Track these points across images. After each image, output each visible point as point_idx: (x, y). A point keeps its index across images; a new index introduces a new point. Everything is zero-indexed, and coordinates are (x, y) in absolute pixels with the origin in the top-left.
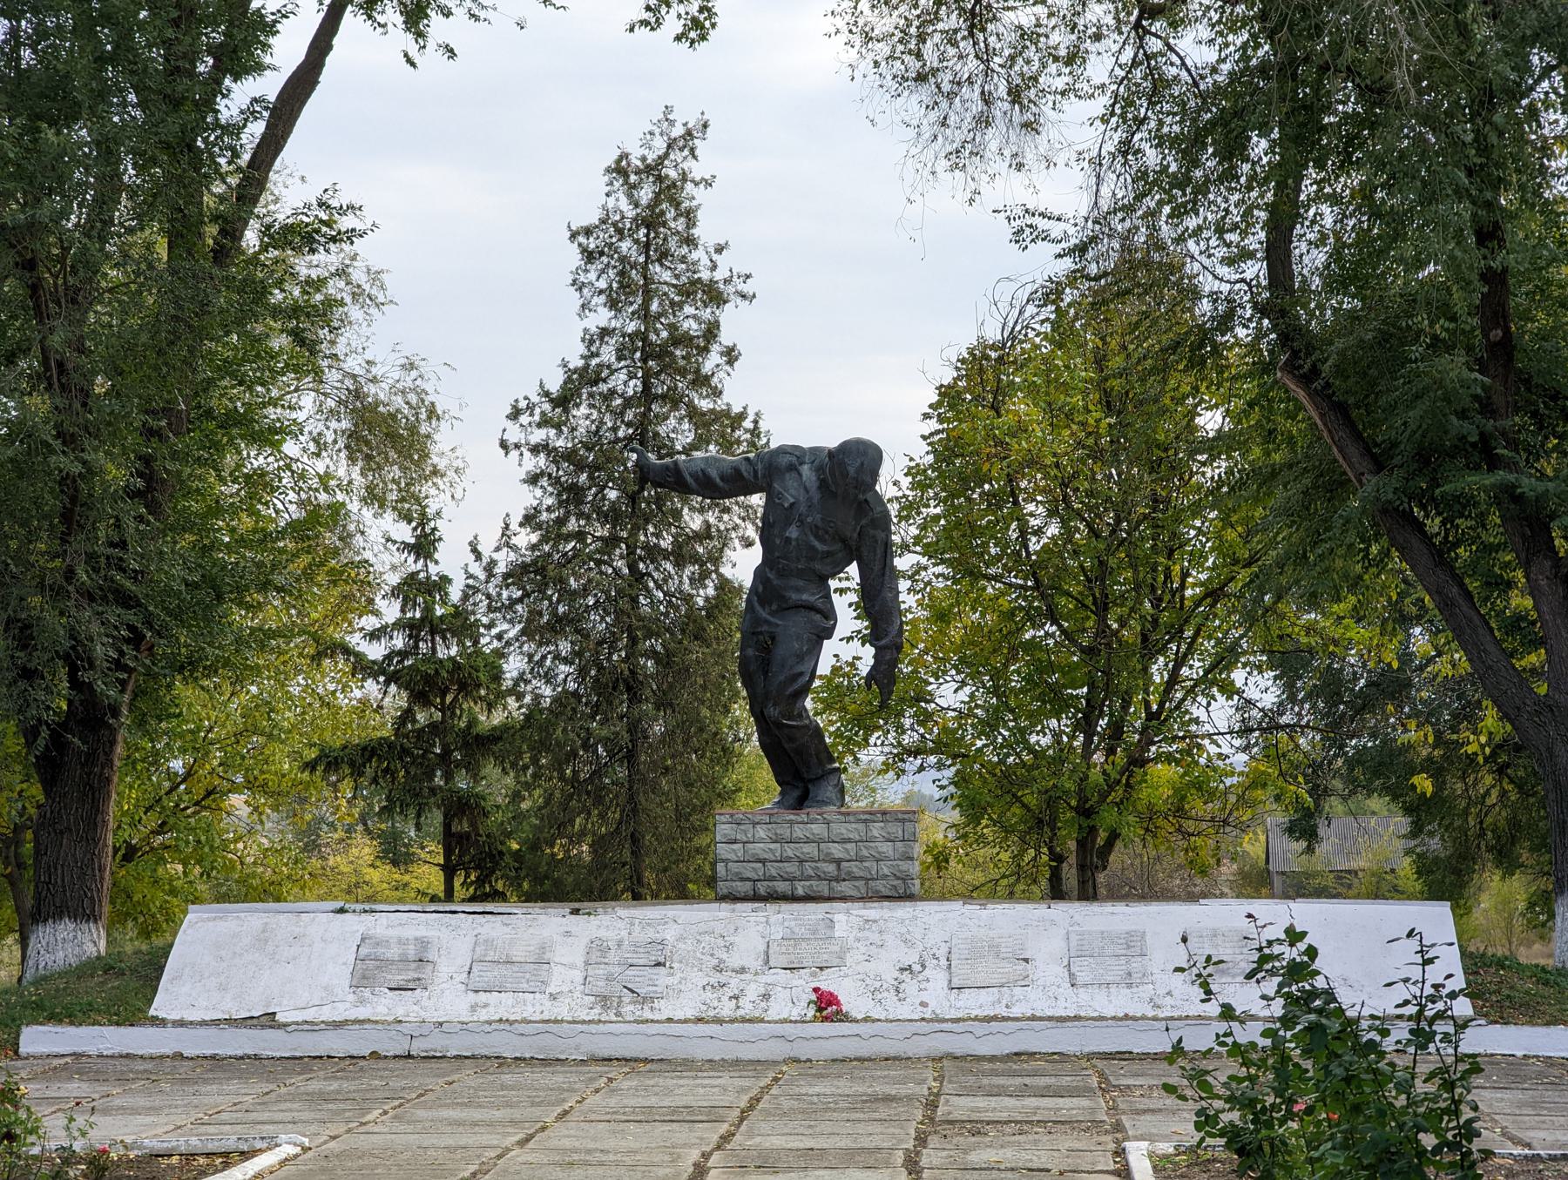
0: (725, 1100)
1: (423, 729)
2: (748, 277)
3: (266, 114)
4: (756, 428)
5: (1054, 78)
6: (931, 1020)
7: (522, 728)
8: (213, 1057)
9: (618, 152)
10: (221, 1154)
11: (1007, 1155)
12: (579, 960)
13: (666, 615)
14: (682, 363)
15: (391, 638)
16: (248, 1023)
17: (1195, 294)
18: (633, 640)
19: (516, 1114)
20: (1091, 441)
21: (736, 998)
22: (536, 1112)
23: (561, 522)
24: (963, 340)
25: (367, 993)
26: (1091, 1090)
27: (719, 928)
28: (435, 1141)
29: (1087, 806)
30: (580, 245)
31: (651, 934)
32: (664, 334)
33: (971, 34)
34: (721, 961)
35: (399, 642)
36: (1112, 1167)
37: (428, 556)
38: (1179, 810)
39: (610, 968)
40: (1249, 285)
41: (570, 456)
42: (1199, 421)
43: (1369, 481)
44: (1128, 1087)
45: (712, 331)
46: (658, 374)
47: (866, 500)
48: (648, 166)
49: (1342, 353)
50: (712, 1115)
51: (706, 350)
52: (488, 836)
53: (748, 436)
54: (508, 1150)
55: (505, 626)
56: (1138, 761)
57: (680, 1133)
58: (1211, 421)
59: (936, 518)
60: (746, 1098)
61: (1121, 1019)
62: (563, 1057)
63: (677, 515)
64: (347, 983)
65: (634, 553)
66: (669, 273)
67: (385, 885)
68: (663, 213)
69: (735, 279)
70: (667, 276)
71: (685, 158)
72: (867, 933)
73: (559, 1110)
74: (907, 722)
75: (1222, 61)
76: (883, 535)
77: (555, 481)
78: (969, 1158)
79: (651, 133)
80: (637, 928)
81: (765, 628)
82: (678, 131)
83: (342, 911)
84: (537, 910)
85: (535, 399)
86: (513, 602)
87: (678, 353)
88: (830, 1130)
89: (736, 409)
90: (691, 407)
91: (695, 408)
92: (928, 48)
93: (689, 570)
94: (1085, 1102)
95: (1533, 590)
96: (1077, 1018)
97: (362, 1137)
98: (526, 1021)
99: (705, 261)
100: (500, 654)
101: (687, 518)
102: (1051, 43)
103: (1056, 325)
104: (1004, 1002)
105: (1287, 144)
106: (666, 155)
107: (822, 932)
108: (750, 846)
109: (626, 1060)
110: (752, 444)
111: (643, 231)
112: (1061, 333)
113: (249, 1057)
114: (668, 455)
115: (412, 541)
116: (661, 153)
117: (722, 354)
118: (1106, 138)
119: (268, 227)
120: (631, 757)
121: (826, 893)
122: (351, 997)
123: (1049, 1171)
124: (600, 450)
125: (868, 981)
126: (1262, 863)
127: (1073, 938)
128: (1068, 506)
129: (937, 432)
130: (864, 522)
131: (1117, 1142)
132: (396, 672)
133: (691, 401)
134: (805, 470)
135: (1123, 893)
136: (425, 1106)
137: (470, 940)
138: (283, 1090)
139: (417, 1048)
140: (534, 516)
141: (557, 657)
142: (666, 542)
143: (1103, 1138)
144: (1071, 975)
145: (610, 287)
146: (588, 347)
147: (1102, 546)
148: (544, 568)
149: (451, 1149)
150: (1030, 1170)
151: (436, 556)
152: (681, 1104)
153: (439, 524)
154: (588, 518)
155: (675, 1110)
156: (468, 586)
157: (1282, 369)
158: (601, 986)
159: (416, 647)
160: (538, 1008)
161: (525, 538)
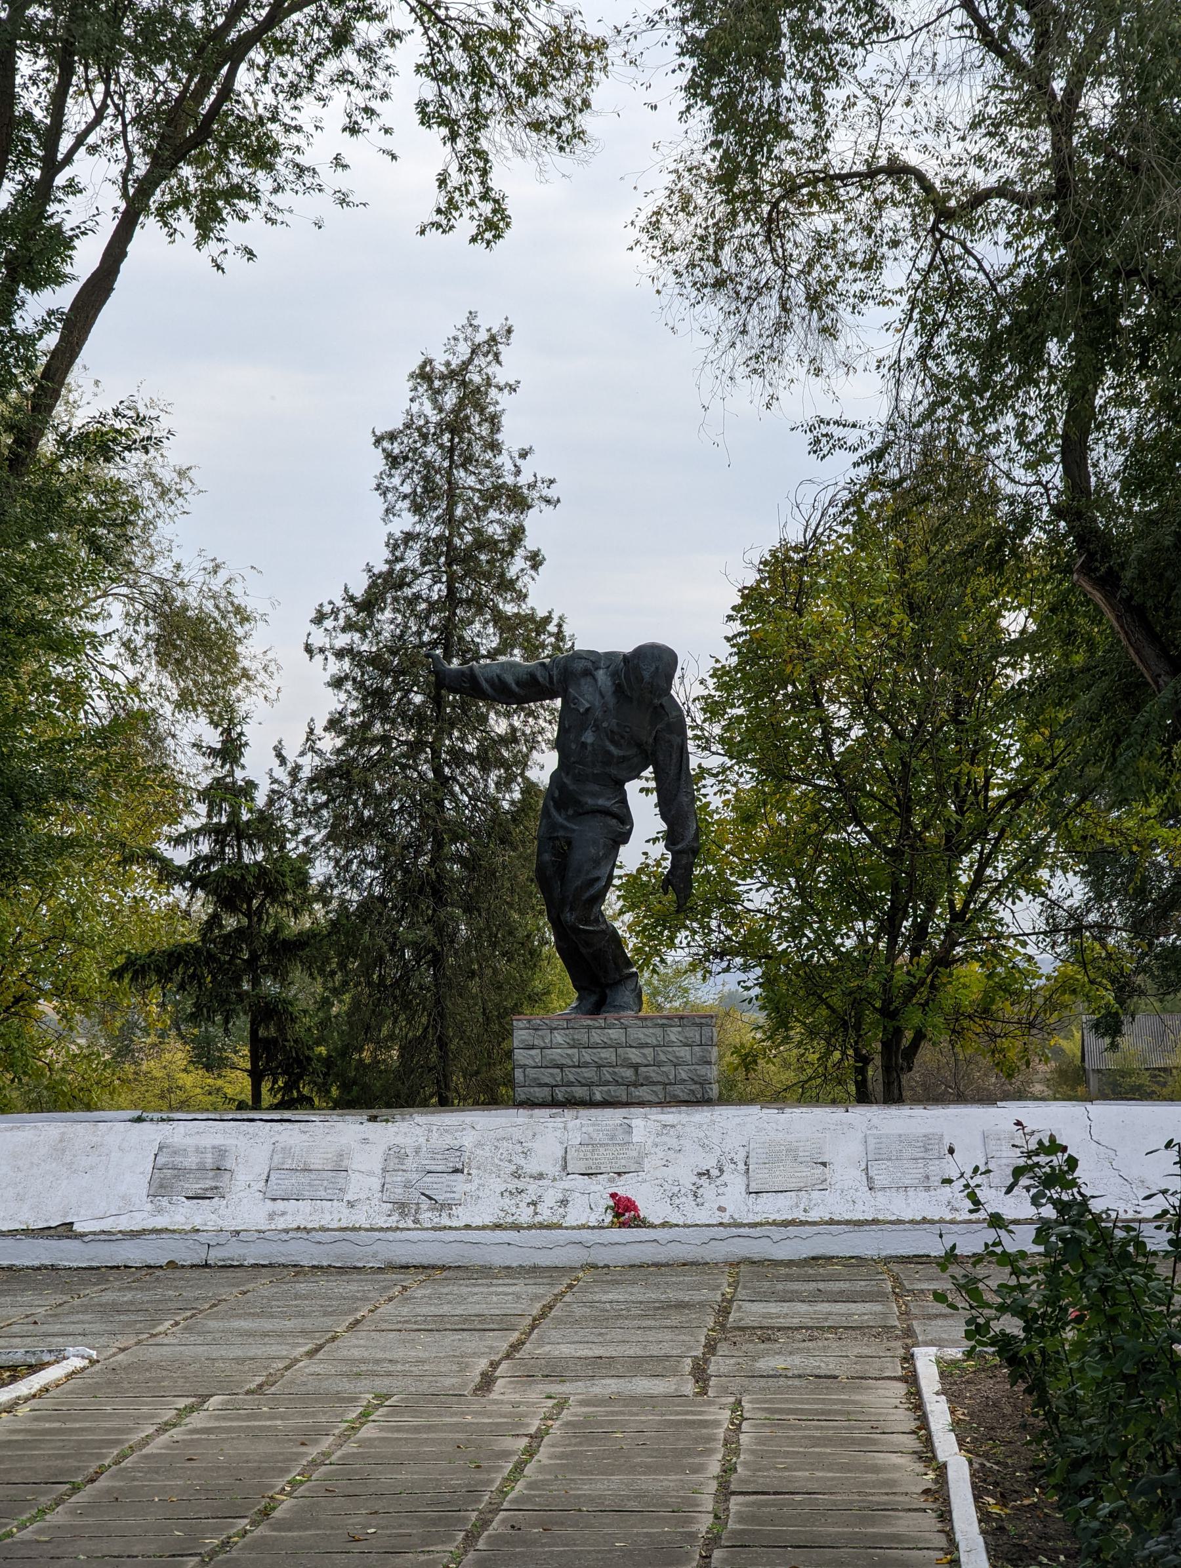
0: (519, 1308)
1: (230, 934)
2: (552, 482)
3: (59, 325)
4: (560, 632)
5: (852, 283)
6: (729, 1225)
7: (329, 934)
8: (10, 1268)
9: (422, 358)
10: (9, 1368)
11: (796, 1362)
12: (377, 1168)
13: (471, 819)
14: (486, 567)
15: (197, 843)
16: (46, 1232)
17: (994, 497)
18: (439, 845)
19: (308, 1324)
20: (893, 642)
21: (534, 1204)
22: (328, 1321)
23: (366, 726)
24: (765, 543)
25: (164, 1202)
26: (884, 1295)
27: (517, 1134)
28: (223, 1353)
29: (892, 1008)
30: (384, 450)
31: (449, 1141)
32: (469, 539)
33: (768, 240)
34: (519, 1167)
35: (205, 847)
36: (900, 1373)
37: (235, 761)
38: (985, 1011)
39: (408, 1175)
40: (1045, 487)
41: (374, 660)
42: (1004, 623)
43: (1166, 684)
44: (922, 1291)
45: (516, 535)
46: (462, 578)
47: (661, 705)
48: (452, 371)
49: (1140, 559)
50: (504, 1324)
51: (511, 554)
52: (296, 1041)
53: (553, 640)
54: (297, 1361)
55: (312, 832)
56: (944, 960)
57: (471, 1343)
58: (1014, 622)
59: (740, 718)
60: (539, 1305)
61: (918, 1223)
62: (360, 1265)
63: (484, 719)
64: (145, 1192)
65: (439, 757)
66: (473, 478)
67: (198, 1090)
68: (467, 418)
69: (539, 484)
70: (471, 481)
71: (489, 363)
72: (664, 1138)
73: (351, 1319)
74: (714, 924)
75: (1017, 265)
76: (679, 740)
77: (360, 685)
78: (757, 1365)
79: (455, 339)
80: (435, 1135)
81: (561, 833)
82: (482, 337)
83: (139, 1120)
84: (335, 1118)
85: (340, 603)
86: (319, 807)
87: (483, 557)
88: (620, 1338)
89: (541, 613)
90: (495, 609)
91: (499, 612)
92: (726, 253)
93: (494, 775)
94: (878, 1308)
96: (875, 1222)
97: (151, 1349)
98: (324, 1229)
99: (509, 466)
100: (306, 859)
101: (492, 722)
102: (848, 249)
103: (858, 528)
104: (802, 1206)
105: (1084, 348)
106: (471, 360)
107: (620, 1137)
108: (548, 1051)
109: (424, 1267)
110: (557, 648)
111: (447, 436)
112: (864, 537)
113: (46, 1268)
114: (472, 659)
115: (219, 746)
116: (465, 357)
117: (526, 558)
118: (906, 343)
119: (63, 436)
120: (437, 962)
121: (624, 1098)
122: (149, 1207)
123: (836, 1377)
124: (405, 654)
125: (666, 1186)
126: (1078, 1062)
127: (871, 1141)
128: (872, 708)
129: (741, 634)
130: (659, 727)
131: (907, 1347)
132: (203, 877)
133: (496, 606)
134: (601, 674)
135: (932, 1096)
136: (215, 1316)
137: (268, 1147)
138: (77, 1301)
139: (214, 1256)
140: (338, 721)
141: (363, 862)
142: (471, 747)
143: (893, 1344)
144: (869, 1179)
145: (415, 491)
146: (392, 552)
147: (905, 747)
148: (348, 772)
149: (240, 1361)
150: (817, 1377)
151: (243, 761)
152: (473, 1312)
153: (246, 729)
154: (393, 722)
155: (466, 1318)
156: (273, 791)
157: (1079, 571)
158: (398, 1193)
159: (223, 852)
160: (336, 1216)
161: (330, 743)
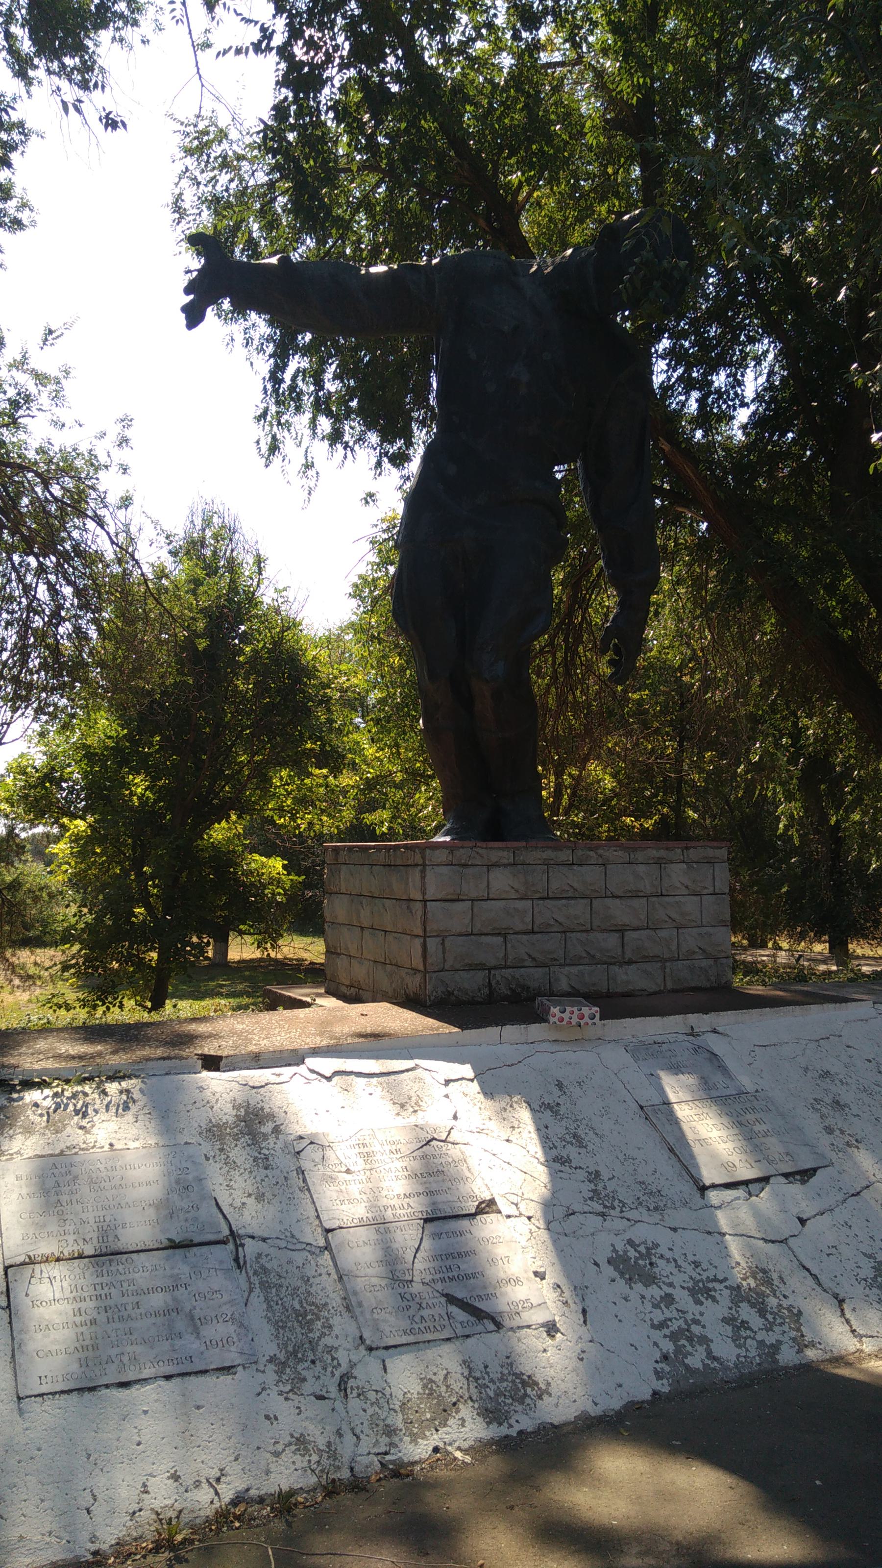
95: (690, 511)
